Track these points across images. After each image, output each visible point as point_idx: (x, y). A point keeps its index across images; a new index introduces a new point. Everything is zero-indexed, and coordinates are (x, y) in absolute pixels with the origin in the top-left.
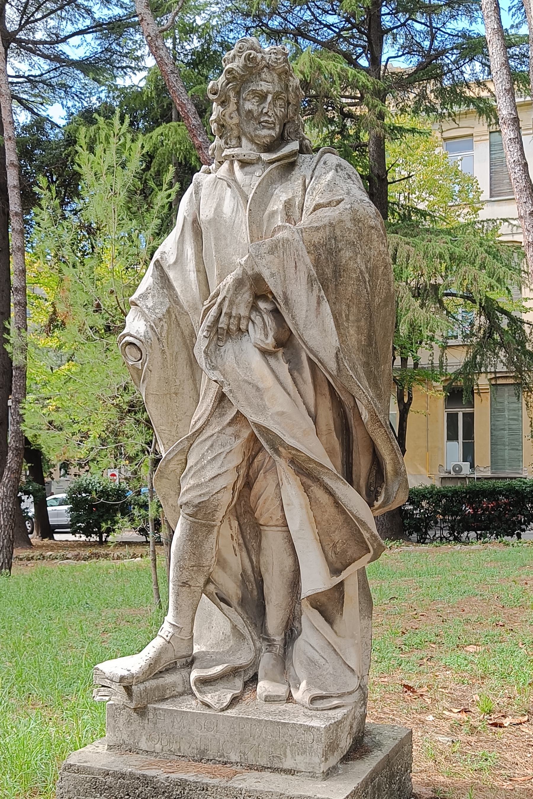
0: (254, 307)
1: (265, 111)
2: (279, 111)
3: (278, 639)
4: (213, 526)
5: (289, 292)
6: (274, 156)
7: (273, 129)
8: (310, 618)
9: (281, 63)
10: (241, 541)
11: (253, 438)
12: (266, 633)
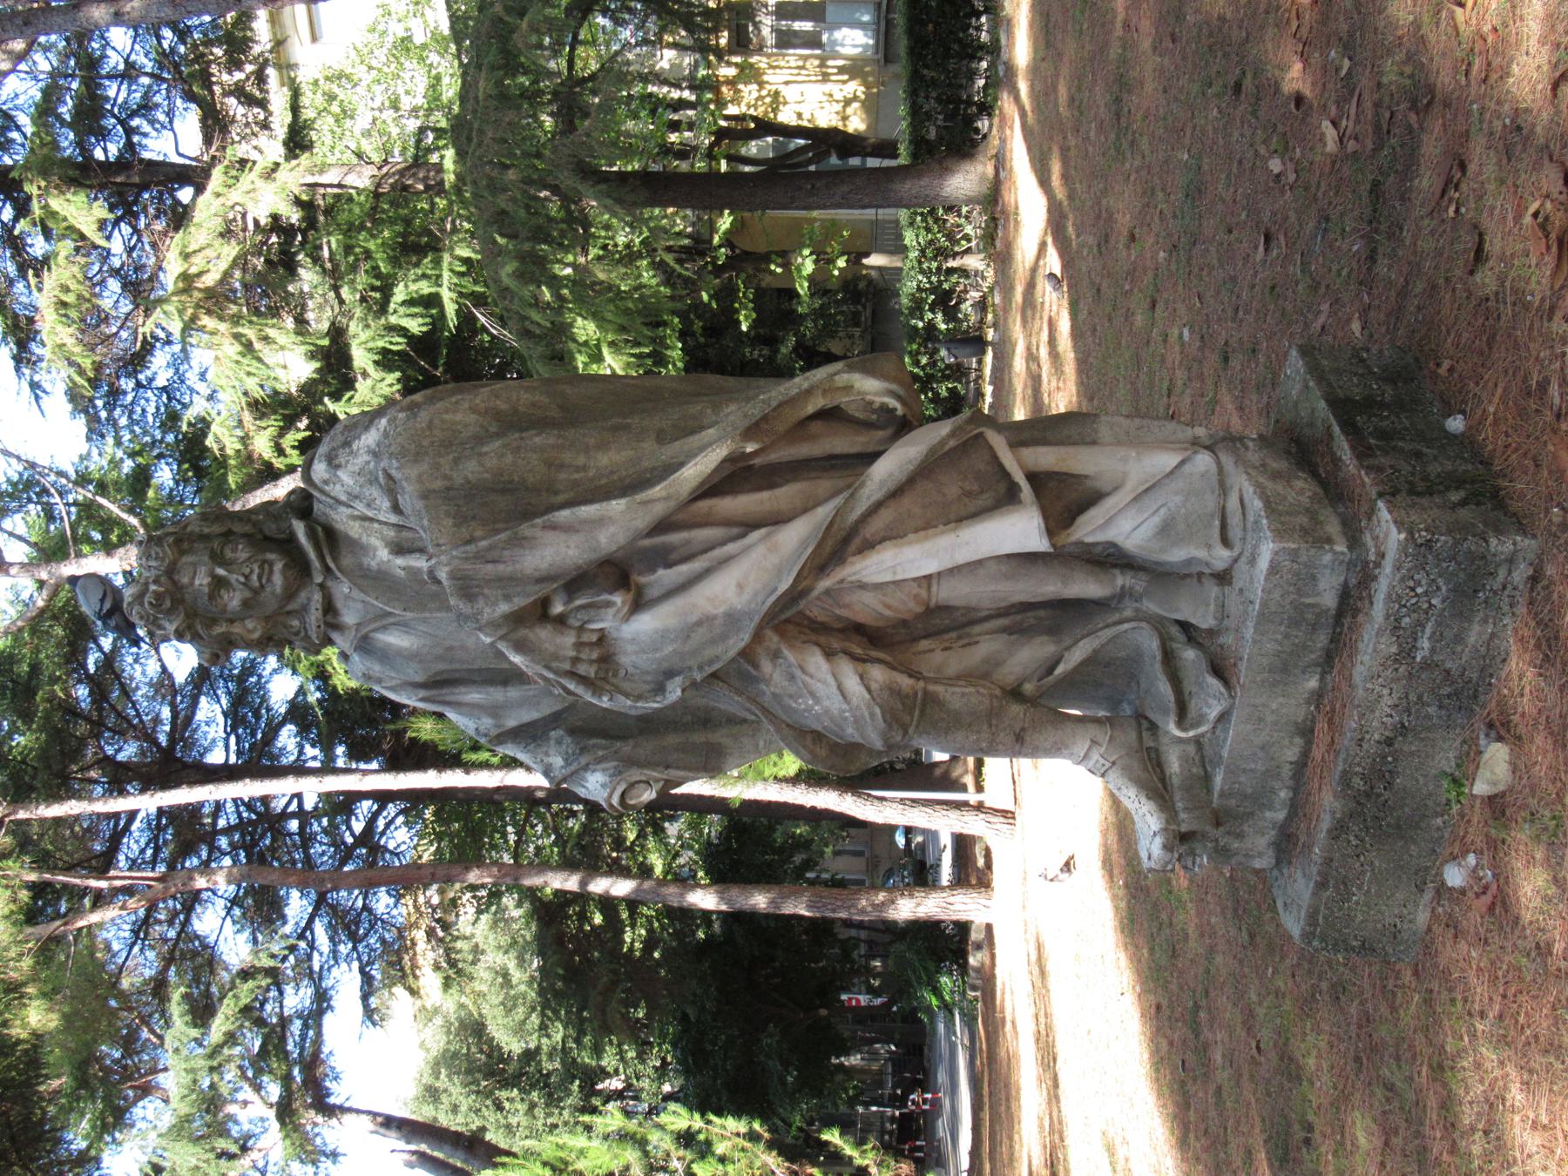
0: (561, 620)
1: (242, 579)
2: (242, 553)
3: (1121, 580)
4: (926, 692)
5: (537, 574)
6: (316, 563)
7: (271, 564)
8: (1090, 529)
9: (164, 552)
10: (954, 635)
11: (780, 630)
12: (1113, 597)
